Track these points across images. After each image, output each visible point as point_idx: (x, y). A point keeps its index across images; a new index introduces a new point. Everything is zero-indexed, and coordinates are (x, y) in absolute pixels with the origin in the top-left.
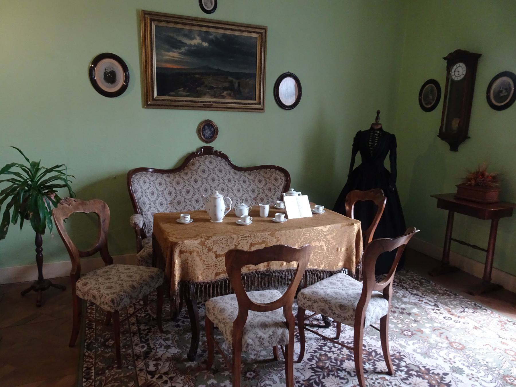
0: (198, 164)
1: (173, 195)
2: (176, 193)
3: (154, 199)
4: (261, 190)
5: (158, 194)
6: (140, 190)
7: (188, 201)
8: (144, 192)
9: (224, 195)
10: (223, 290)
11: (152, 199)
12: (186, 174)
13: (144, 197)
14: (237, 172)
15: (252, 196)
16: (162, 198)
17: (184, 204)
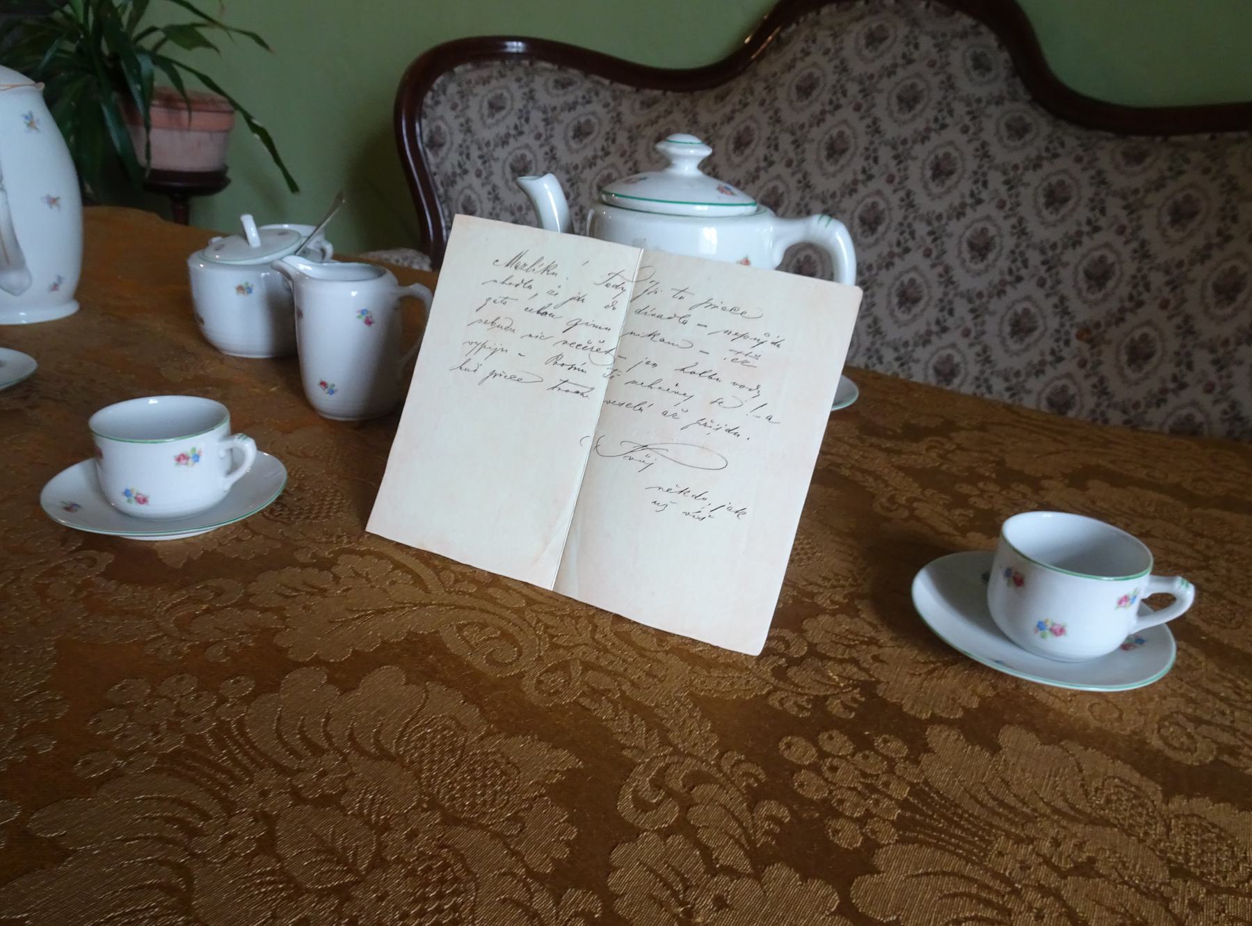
0: (899, 49)
1: (1119, 289)
2: (1140, 281)
3: (980, 284)
4: (1034, 258)
5: (1018, 256)
6: (459, 138)
7: (1202, 359)
8: (475, 153)
9: (871, 257)
10: (497, 610)
11: (966, 282)
12: (1018, 130)
13: (471, 178)
14: (1042, 125)
15: (1074, 304)
16: (924, 264)
17: (1168, 369)
